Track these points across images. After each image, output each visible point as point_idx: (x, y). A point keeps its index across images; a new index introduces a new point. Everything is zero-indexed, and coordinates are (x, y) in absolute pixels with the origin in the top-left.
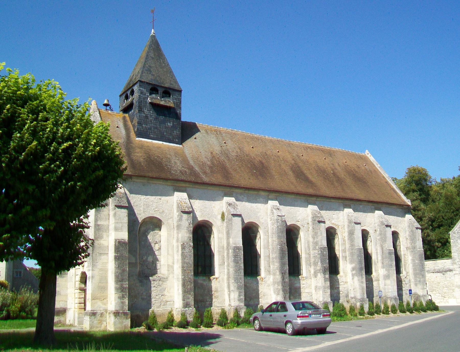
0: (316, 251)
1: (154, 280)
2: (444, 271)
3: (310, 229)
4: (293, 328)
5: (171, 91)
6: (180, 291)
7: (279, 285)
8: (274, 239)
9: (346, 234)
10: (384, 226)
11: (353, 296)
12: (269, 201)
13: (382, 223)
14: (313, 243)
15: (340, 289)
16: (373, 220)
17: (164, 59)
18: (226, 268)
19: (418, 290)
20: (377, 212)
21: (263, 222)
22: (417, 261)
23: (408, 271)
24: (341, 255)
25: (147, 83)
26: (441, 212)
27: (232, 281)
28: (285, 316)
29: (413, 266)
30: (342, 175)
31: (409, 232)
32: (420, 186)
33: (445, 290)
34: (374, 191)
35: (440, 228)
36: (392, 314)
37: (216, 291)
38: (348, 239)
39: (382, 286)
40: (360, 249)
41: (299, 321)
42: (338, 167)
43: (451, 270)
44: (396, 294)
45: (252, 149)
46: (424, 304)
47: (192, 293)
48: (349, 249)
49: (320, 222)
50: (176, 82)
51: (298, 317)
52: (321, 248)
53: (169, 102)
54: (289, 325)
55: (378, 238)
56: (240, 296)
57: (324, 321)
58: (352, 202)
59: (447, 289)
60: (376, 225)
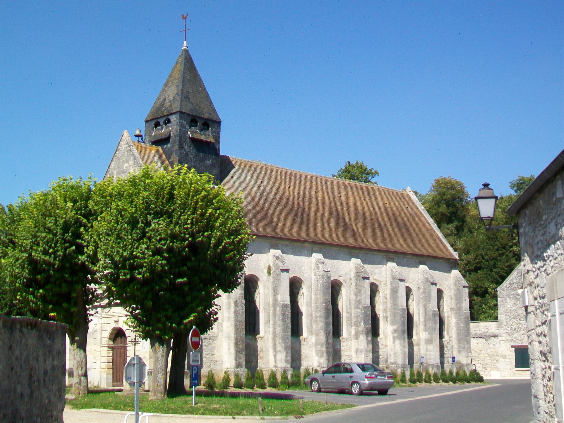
0: (359, 310)
1: (205, 339)
2: (487, 337)
3: (352, 286)
4: (360, 388)
5: (210, 123)
6: (233, 350)
7: (322, 347)
8: (319, 296)
9: (388, 292)
10: (430, 284)
11: (393, 361)
12: (314, 254)
13: (427, 280)
14: (355, 301)
15: (380, 353)
16: (416, 275)
17: (200, 80)
18: (271, 326)
19: (462, 359)
20: (421, 266)
21: (307, 276)
22: (462, 325)
23: (451, 335)
24: (381, 315)
25: (187, 114)
26: (481, 248)
27: (279, 341)
28: (351, 377)
29: (457, 330)
30: (384, 220)
31: (455, 291)
32: (452, 209)
33: (487, 360)
34: (419, 242)
35: (477, 272)
36: (435, 383)
37: (262, 351)
38: (391, 298)
39: (423, 352)
40: (403, 309)
41: (367, 381)
42: (378, 211)
43: (495, 336)
44: (438, 361)
45: (288, 189)
46: (468, 373)
47: (244, 353)
48: (390, 309)
49: (364, 278)
50: (215, 111)
51: (366, 377)
52: (365, 307)
53: (207, 136)
54: (355, 386)
55: (421, 296)
56: (286, 357)
57: (388, 382)
58: (395, 255)
59: (489, 358)
60: (420, 281)
